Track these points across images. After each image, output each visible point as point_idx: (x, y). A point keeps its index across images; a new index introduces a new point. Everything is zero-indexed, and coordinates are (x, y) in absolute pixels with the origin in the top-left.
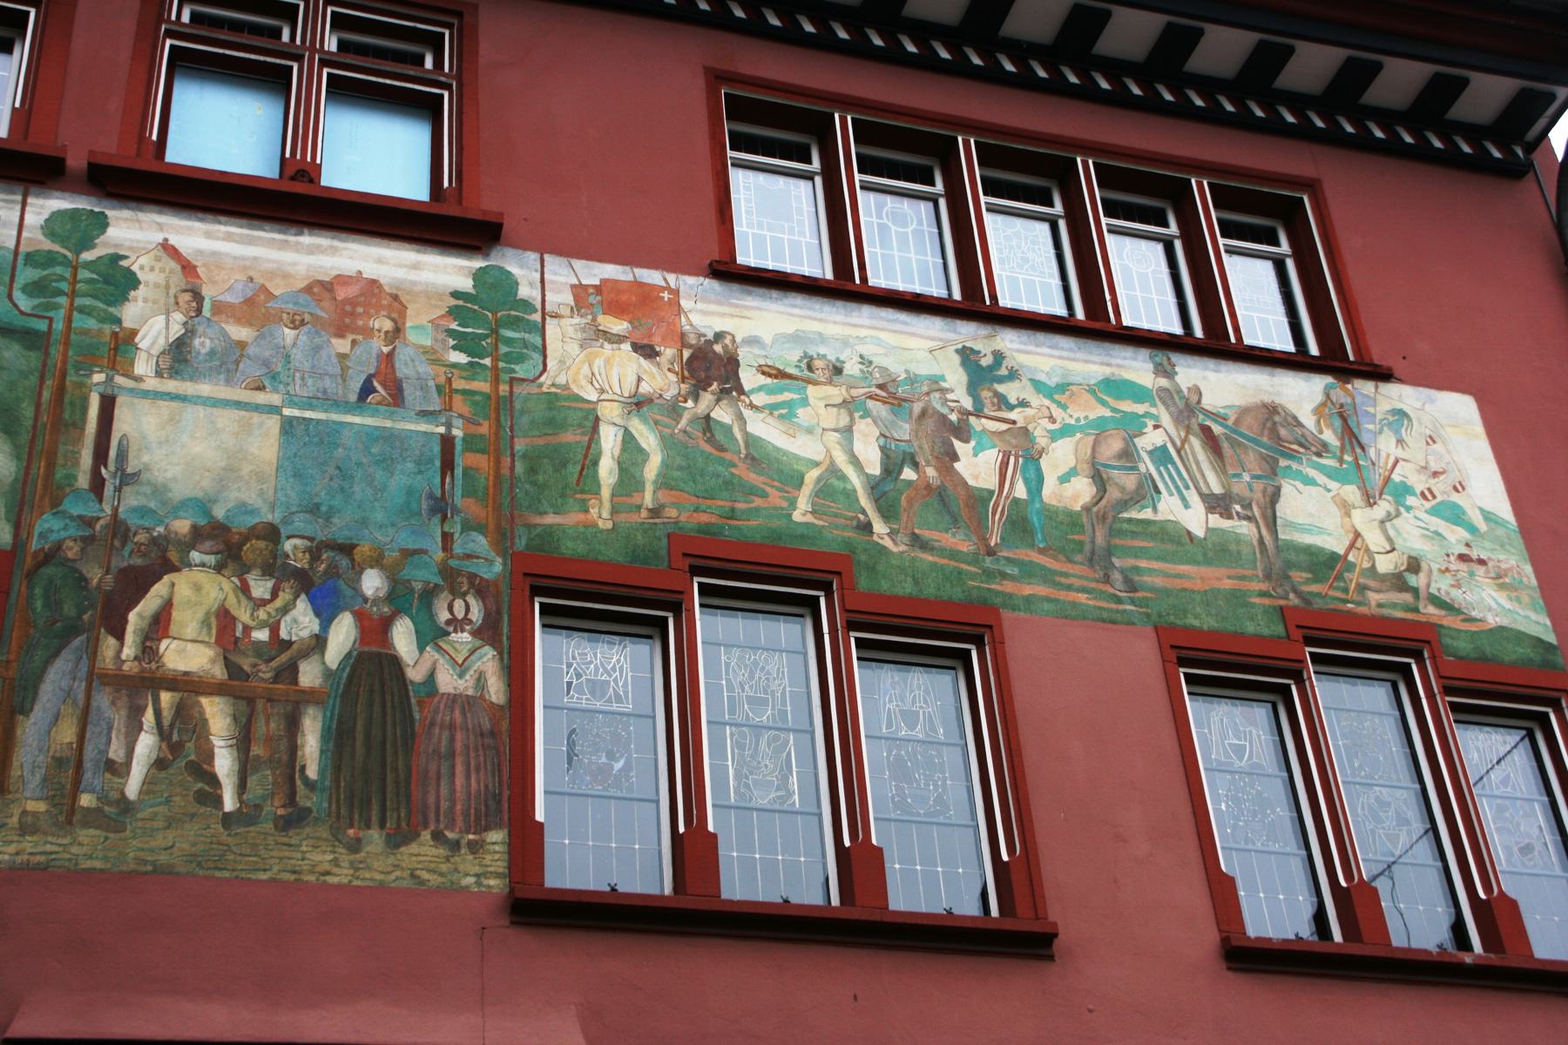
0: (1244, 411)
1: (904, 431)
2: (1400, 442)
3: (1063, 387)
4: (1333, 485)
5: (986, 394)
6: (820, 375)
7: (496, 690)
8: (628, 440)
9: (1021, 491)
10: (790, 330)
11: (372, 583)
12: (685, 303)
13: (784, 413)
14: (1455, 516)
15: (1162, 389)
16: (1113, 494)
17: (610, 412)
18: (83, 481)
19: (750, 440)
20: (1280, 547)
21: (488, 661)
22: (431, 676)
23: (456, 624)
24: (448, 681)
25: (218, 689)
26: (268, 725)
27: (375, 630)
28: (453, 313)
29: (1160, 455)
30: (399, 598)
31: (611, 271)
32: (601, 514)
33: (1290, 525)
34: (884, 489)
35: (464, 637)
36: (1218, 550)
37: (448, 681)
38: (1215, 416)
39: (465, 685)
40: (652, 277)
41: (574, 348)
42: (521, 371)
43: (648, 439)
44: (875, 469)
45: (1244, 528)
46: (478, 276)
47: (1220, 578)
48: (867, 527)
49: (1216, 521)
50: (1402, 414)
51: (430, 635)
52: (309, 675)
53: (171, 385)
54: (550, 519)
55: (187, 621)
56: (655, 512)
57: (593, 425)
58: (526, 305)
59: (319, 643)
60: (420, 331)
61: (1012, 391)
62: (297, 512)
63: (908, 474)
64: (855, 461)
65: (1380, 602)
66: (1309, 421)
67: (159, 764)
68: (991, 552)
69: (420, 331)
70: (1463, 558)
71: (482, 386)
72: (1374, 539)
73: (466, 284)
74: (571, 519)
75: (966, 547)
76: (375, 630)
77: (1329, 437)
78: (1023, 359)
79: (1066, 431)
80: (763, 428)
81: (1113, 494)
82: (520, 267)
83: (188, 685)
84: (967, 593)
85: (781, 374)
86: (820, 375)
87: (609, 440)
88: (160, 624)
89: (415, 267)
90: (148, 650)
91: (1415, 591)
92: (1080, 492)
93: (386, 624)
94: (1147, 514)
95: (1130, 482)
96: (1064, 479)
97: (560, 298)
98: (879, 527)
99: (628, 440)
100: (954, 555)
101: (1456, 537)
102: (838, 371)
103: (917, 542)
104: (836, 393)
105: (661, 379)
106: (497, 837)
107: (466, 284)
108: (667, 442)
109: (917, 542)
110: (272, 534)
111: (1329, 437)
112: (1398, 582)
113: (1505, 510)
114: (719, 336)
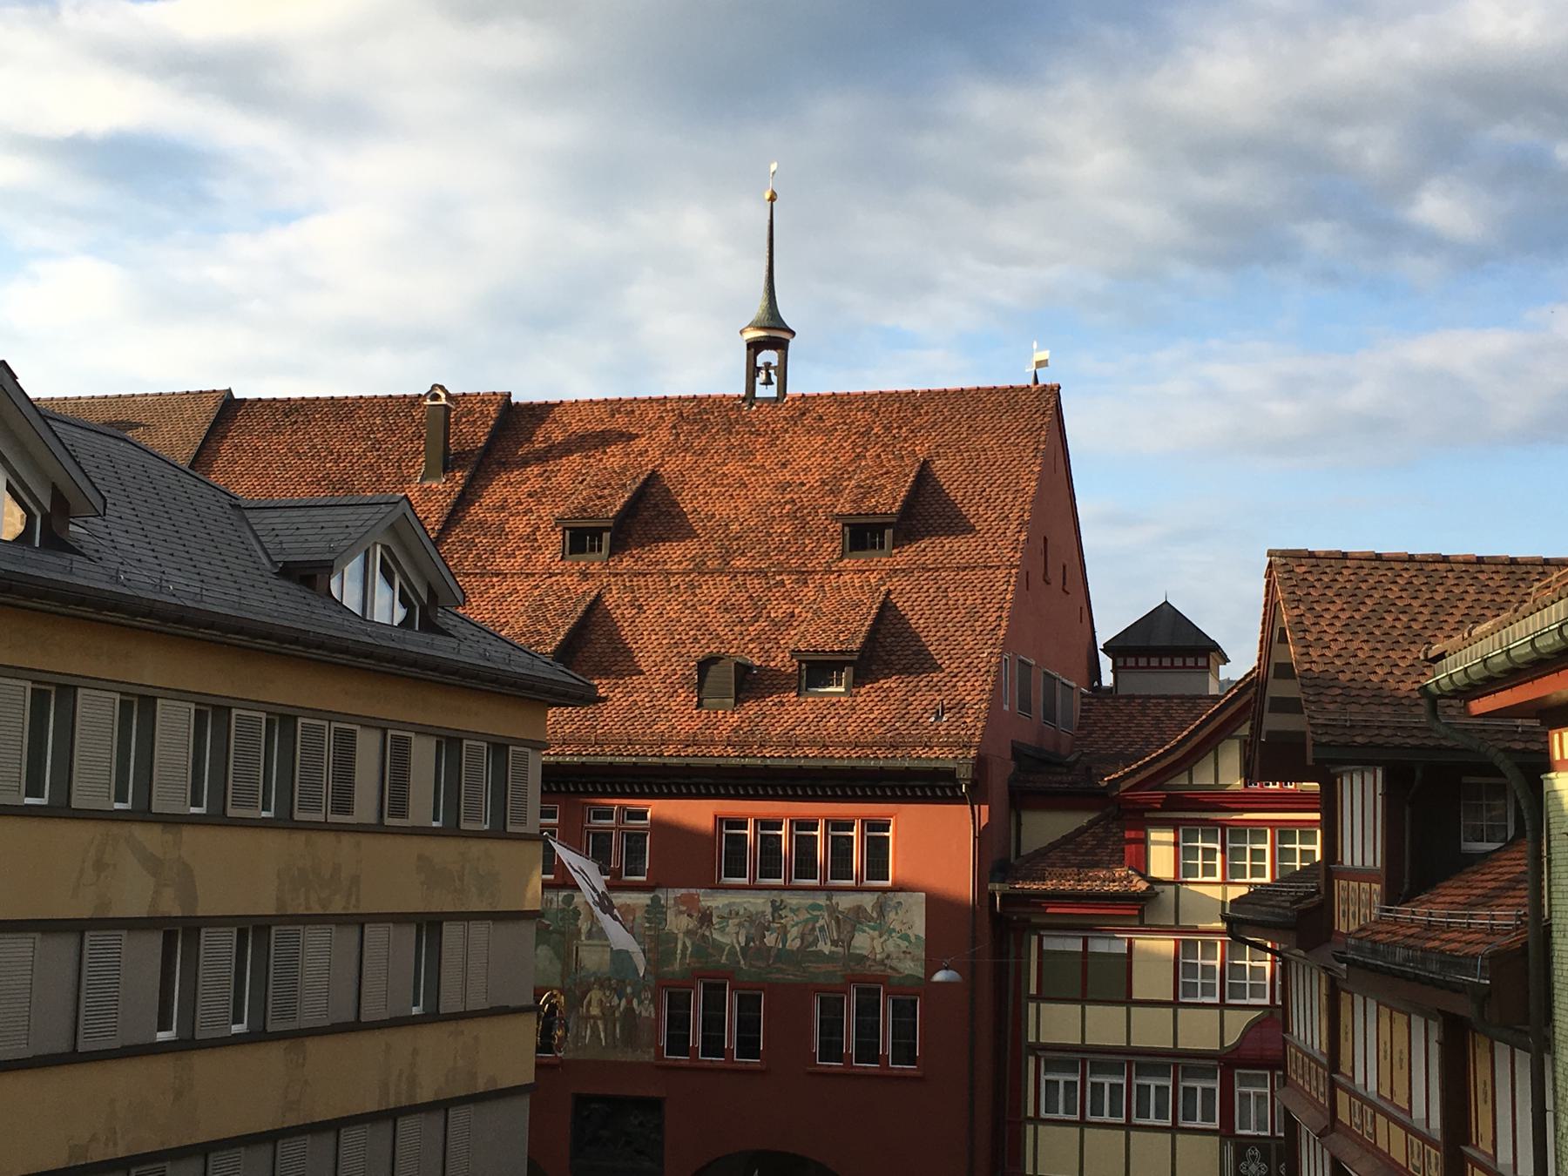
0: (850, 909)
1: (753, 931)
2: (897, 913)
3: (798, 909)
4: (871, 932)
5: (776, 915)
6: (733, 915)
7: (653, 1015)
8: (684, 943)
9: (781, 946)
10: (727, 902)
11: (629, 990)
12: (701, 899)
13: (722, 930)
14: (905, 937)
15: (827, 905)
16: (806, 943)
17: (681, 936)
18: (574, 970)
19: (714, 940)
20: (850, 954)
21: (652, 1008)
22: (640, 1012)
23: (646, 999)
24: (644, 1014)
25: (600, 1019)
26: (610, 1026)
27: (630, 1002)
28: (646, 911)
29: (822, 929)
30: (634, 994)
31: (683, 891)
32: (677, 966)
33: (855, 948)
34: (745, 950)
35: (647, 1002)
36: (832, 957)
37: (644, 1014)
38: (841, 912)
39: (647, 1015)
40: (693, 891)
41: (673, 918)
42: (661, 927)
43: (689, 944)
44: (743, 944)
45: (840, 949)
46: (652, 899)
47: (829, 967)
48: (739, 962)
49: (833, 949)
50: (900, 903)
51: (640, 1003)
52: (617, 1014)
53: (590, 942)
54: (666, 969)
55: (594, 1003)
56: (689, 964)
57: (676, 939)
58: (663, 907)
59: (619, 1005)
60: (639, 914)
61: (783, 913)
62: (464, 501)
63: (752, 944)
64: (739, 943)
65: (877, 969)
66: (869, 910)
67: (591, 1036)
68: (769, 966)
69: (639, 914)
70: (904, 952)
71: (652, 933)
72: (878, 950)
73: (649, 902)
74: (670, 969)
75: (763, 965)
76: (630, 1002)
77: (875, 915)
78: (789, 901)
79: (797, 924)
80: (716, 936)
81: (806, 943)
82: (661, 894)
83: (594, 1017)
84: (855, 691)
85: (723, 917)
86: (733, 915)
87: (680, 946)
88: (590, 1003)
89: (638, 898)
90: (588, 1010)
91: (885, 965)
92: (798, 943)
93: (632, 1001)
94: (814, 948)
95: (811, 939)
96: (793, 940)
97: (671, 902)
98: (742, 962)
99: (684, 943)
100: (759, 968)
101: (904, 944)
102: (737, 914)
103: (752, 966)
104: (736, 921)
105: (692, 924)
106: (652, 1050)
107: (649, 902)
108: (693, 944)
109: (752, 966)
110: (609, 979)
111: (875, 915)
112: (882, 962)
113: (923, 935)
114: (708, 908)
